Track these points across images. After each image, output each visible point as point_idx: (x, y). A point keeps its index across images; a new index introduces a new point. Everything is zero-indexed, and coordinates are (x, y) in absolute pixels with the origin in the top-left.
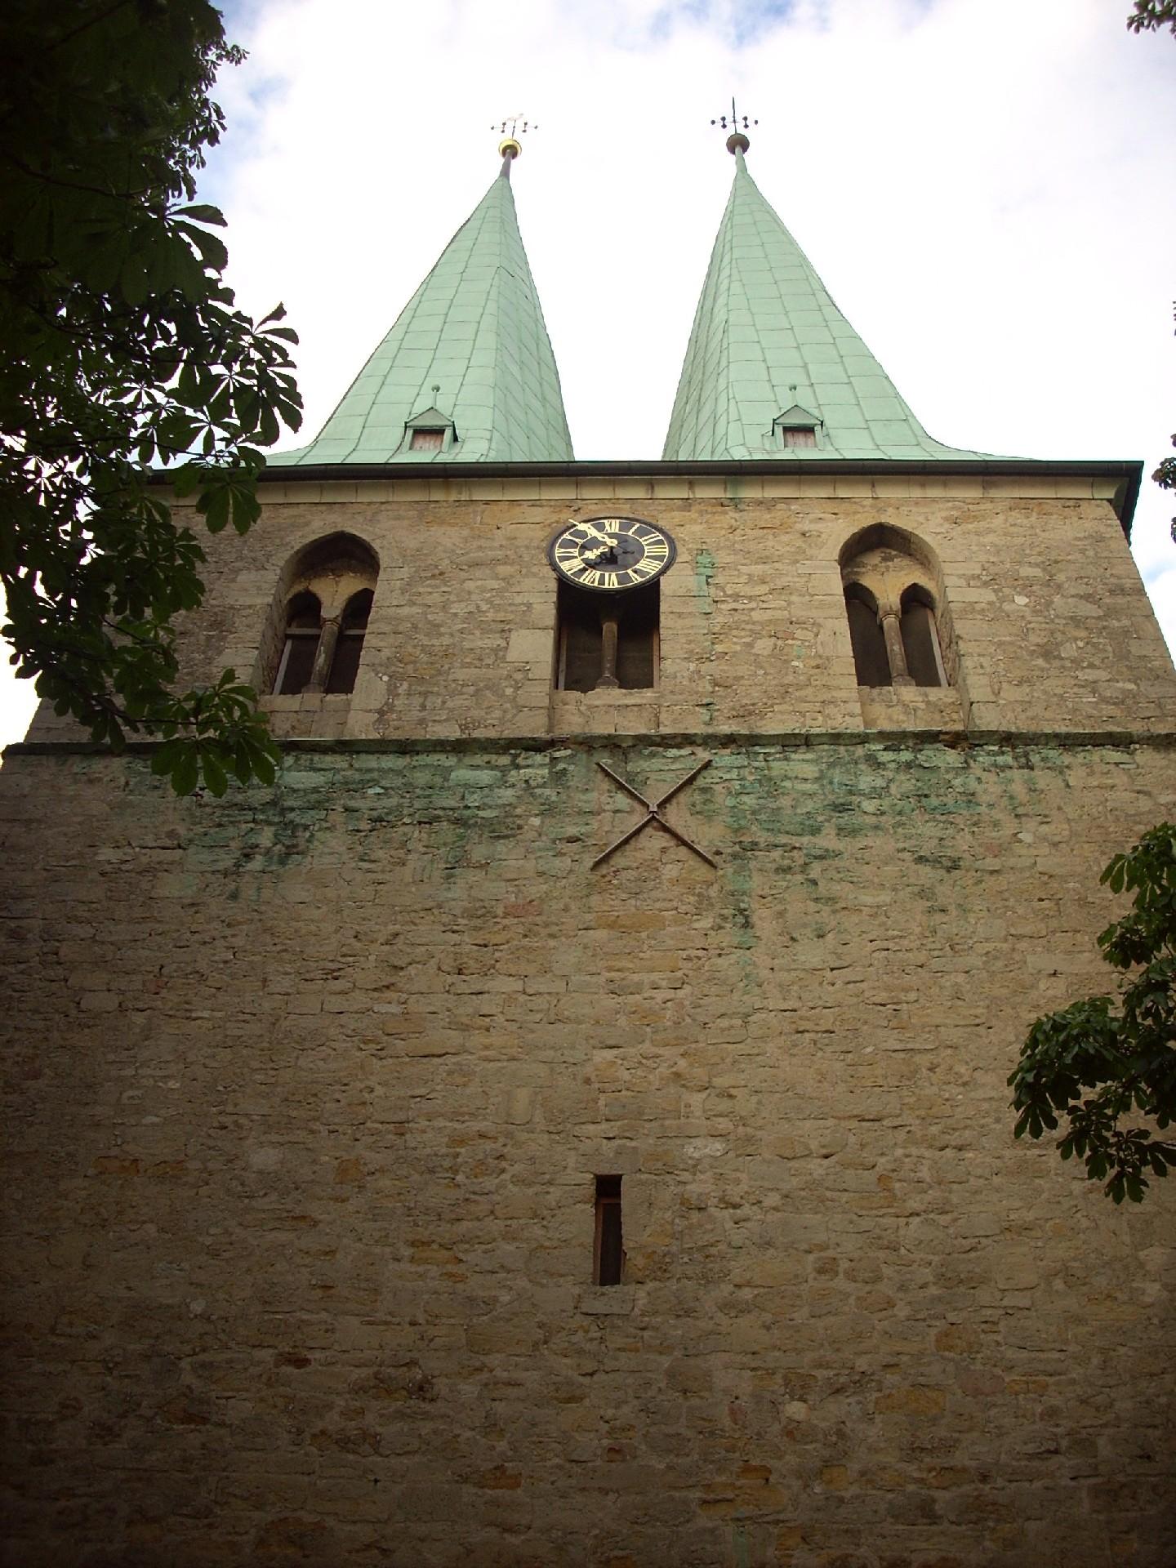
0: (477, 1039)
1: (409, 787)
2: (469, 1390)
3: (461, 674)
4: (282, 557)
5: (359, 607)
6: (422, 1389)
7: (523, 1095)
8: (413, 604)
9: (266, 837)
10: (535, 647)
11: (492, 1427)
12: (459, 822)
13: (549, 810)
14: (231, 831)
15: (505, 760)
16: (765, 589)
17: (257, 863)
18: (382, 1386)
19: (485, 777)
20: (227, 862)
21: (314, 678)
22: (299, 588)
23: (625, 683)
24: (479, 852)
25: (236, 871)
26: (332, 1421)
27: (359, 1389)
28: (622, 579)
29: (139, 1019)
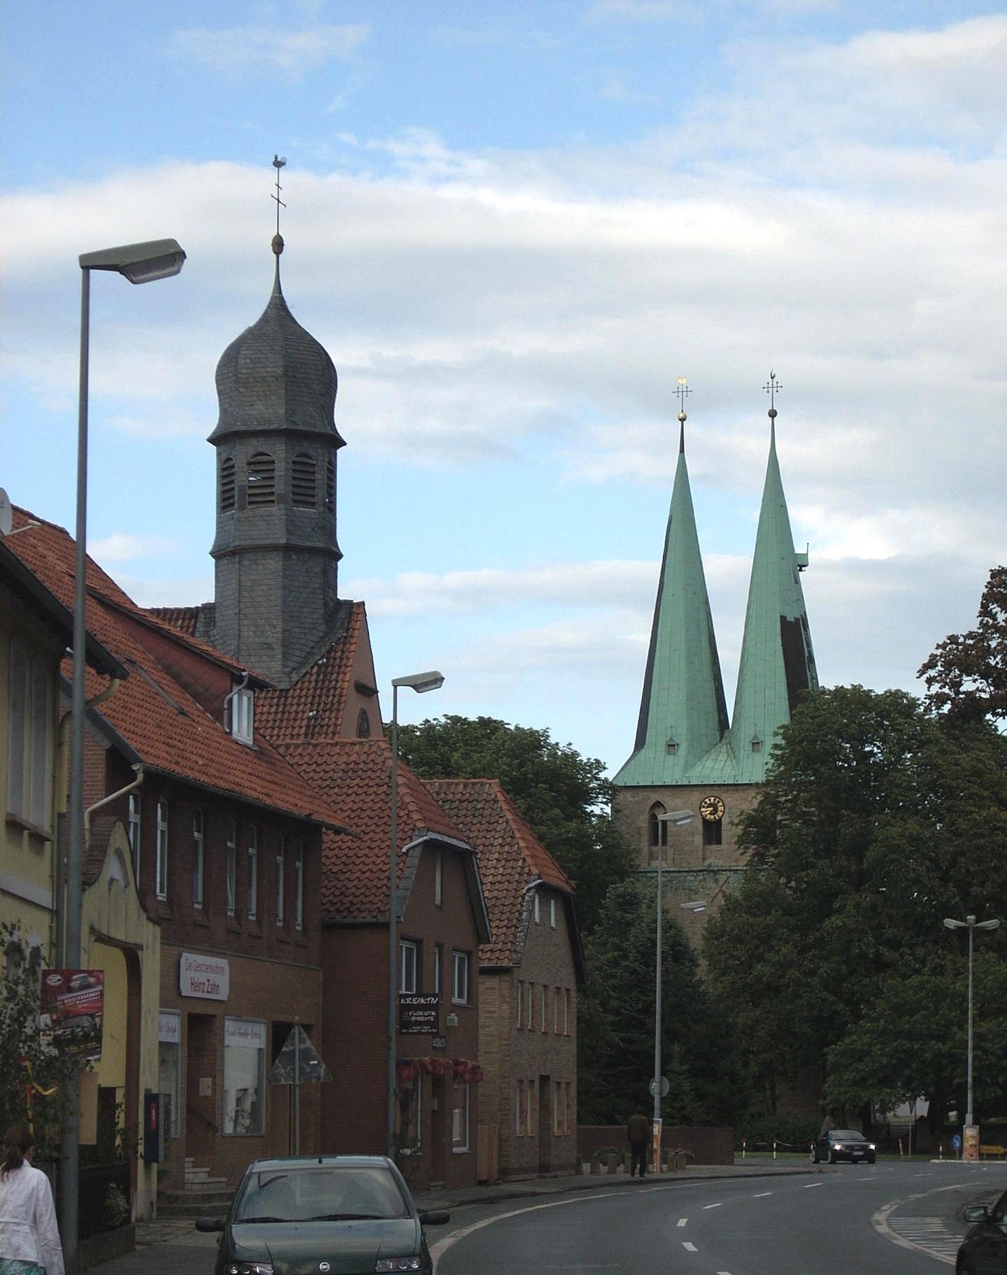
10: (699, 839)
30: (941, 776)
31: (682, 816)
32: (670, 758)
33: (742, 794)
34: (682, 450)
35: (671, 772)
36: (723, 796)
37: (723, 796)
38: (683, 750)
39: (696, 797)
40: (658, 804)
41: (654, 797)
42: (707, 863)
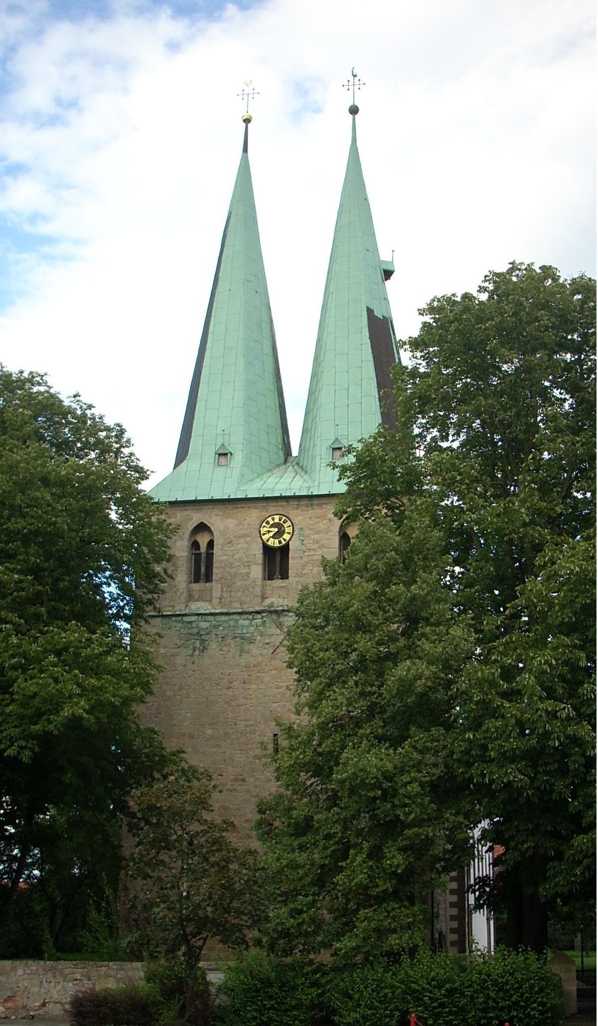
0: (249, 701)
1: (229, 626)
2: (252, 780)
3: (239, 583)
4: (188, 533)
5: (211, 544)
6: (243, 780)
7: (259, 715)
8: (224, 555)
9: (198, 644)
10: (257, 571)
11: (256, 787)
12: (242, 638)
13: (262, 635)
14: (189, 642)
15: (251, 617)
16: (316, 546)
17: (197, 653)
18: (237, 780)
19: (247, 622)
20: (190, 652)
21: (202, 577)
22: (193, 540)
23: (282, 578)
24: (246, 648)
25: (192, 655)
26: (229, 787)
27: (232, 781)
28: (280, 542)
29: (178, 697)
30: (108, 903)
31: (238, 546)
32: (221, 471)
33: (319, 511)
34: (245, 149)
35: (224, 484)
36: (292, 513)
37: (292, 513)
38: (238, 459)
39: (253, 515)
40: (202, 528)
41: (196, 517)
42: (267, 602)
